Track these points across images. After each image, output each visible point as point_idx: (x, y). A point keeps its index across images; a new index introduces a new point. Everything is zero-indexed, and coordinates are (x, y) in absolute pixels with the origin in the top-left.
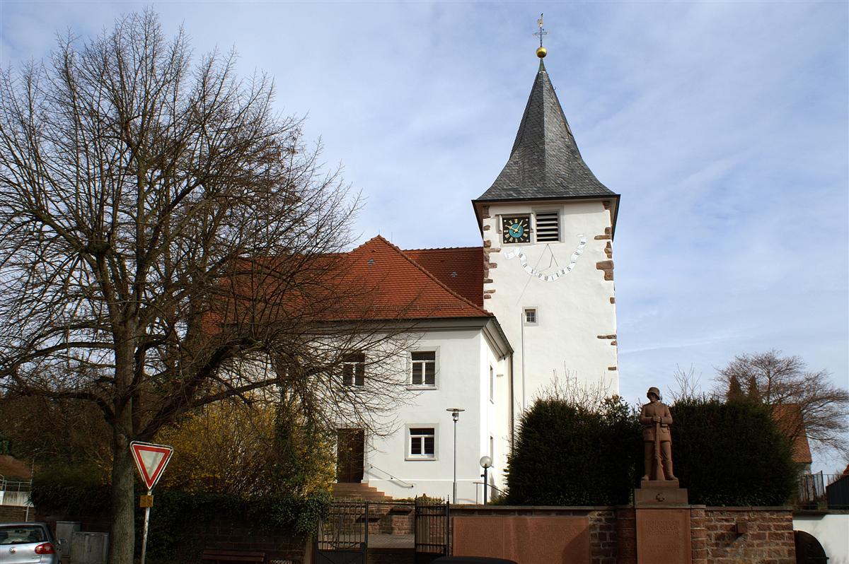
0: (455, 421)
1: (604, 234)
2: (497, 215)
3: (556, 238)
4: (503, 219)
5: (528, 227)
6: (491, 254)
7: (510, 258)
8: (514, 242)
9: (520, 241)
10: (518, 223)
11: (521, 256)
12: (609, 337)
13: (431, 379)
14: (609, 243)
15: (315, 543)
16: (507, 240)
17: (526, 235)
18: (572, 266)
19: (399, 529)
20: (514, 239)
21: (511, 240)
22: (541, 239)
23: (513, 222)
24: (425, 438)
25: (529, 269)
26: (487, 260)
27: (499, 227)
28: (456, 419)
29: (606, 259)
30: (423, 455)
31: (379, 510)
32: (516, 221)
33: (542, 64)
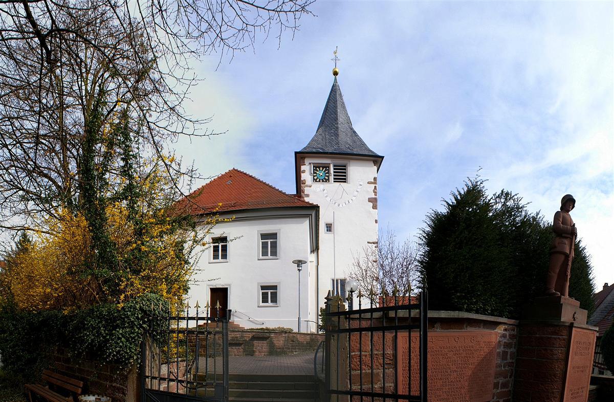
0: (299, 270)
1: (373, 181)
2: (310, 164)
3: (344, 180)
4: (314, 167)
5: (328, 173)
6: (306, 189)
7: (318, 191)
8: (319, 181)
9: (323, 181)
10: (322, 170)
11: (324, 190)
12: (374, 243)
13: (274, 253)
14: (375, 187)
15: (142, 377)
16: (315, 180)
17: (327, 178)
18: (354, 198)
19: (260, 352)
20: (320, 180)
21: (318, 180)
22: (336, 180)
23: (319, 169)
24: (271, 293)
25: (328, 199)
26: (303, 192)
27: (311, 171)
28: (300, 269)
29: (373, 196)
30: (270, 304)
31: (242, 337)
32: (321, 169)
33: (336, 79)
